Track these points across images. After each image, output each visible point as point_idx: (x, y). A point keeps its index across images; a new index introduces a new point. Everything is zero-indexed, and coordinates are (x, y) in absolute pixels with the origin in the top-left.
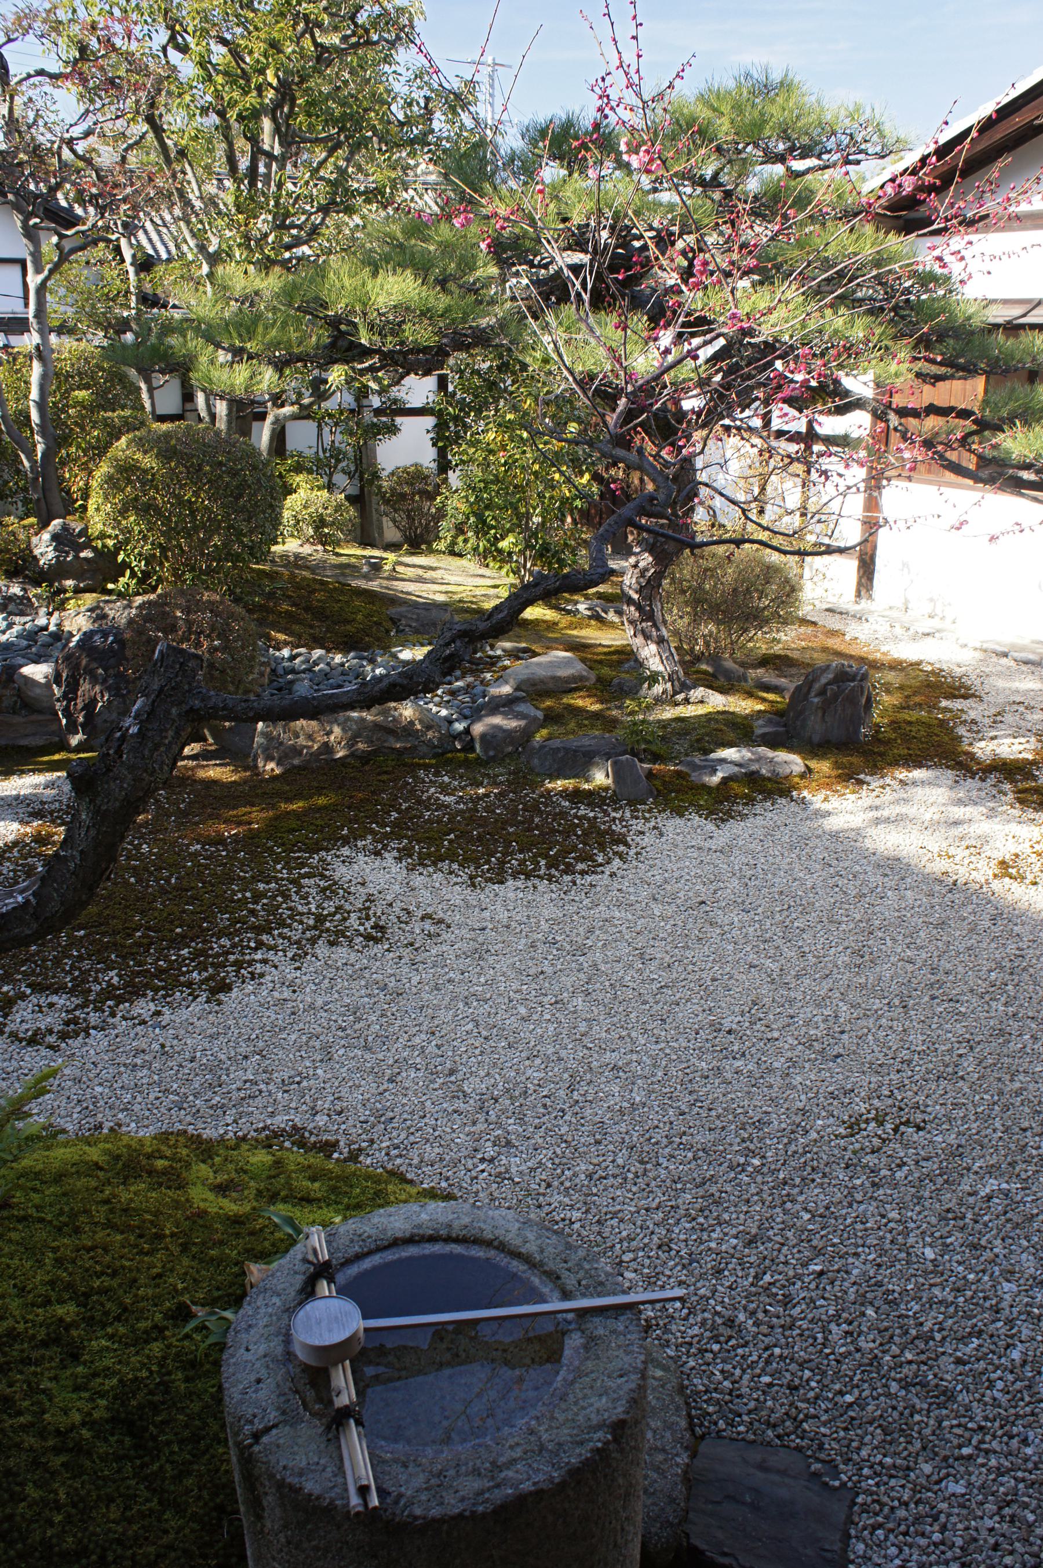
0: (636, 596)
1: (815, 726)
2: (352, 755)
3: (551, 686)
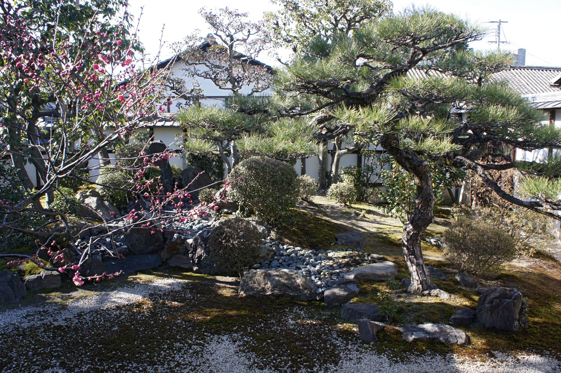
0: (406, 243)
1: (486, 318)
2: (272, 294)
3: (372, 278)
